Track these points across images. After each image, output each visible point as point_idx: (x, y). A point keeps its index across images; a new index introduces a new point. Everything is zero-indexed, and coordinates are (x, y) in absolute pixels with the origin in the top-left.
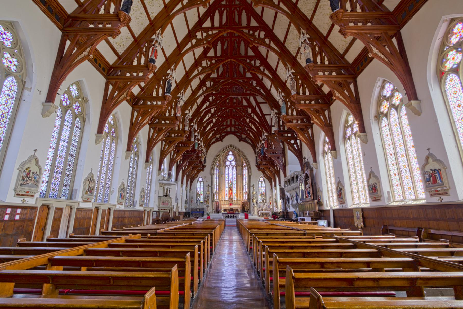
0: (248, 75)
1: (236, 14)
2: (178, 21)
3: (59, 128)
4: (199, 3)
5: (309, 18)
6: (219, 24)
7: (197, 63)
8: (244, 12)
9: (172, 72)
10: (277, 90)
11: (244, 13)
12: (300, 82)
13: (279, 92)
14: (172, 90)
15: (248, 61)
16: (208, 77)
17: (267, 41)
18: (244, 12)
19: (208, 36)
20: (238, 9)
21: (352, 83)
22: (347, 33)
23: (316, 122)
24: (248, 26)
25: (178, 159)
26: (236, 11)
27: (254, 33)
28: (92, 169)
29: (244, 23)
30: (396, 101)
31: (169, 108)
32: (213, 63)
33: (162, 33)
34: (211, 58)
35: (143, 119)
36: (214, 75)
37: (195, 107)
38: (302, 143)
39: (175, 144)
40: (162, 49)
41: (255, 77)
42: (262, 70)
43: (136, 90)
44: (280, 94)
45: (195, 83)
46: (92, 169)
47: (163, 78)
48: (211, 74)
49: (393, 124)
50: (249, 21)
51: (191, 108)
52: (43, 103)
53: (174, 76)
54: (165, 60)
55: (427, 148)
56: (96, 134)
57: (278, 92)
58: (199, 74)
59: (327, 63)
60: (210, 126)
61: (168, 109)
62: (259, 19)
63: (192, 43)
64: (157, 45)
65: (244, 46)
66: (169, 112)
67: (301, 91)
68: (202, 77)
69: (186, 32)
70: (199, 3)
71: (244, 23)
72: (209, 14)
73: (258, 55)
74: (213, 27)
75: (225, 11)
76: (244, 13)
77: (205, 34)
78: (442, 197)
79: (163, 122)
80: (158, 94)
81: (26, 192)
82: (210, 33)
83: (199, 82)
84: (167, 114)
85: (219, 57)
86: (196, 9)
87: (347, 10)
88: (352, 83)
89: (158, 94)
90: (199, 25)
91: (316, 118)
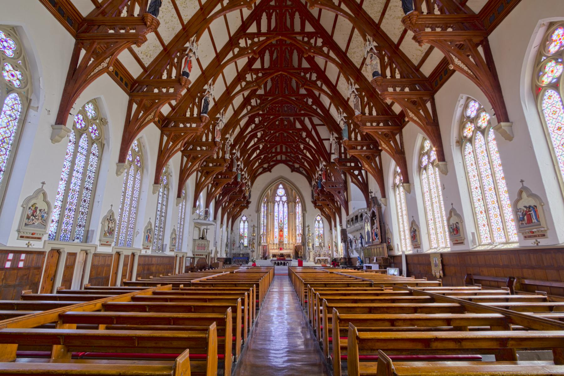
0: (303, 91)
1: (288, 17)
2: (217, 25)
3: (71, 156)
4: (242, 3)
5: (377, 22)
6: (267, 29)
7: (240, 77)
8: (297, 14)
9: (210, 87)
10: (338, 109)
11: (297, 16)
12: (366, 99)
13: (340, 112)
14: (209, 110)
15: (302, 74)
16: (253, 94)
17: (325, 49)
18: (297, 14)
19: (253, 44)
20: (290, 11)
21: (429, 102)
22: (422, 40)
23: (385, 148)
24: (303, 32)
25: (217, 194)
26: (288, 14)
27: (309, 41)
28: (112, 206)
29: (298, 28)
30: (482, 123)
31: (206, 131)
32: (259, 77)
33: (197, 40)
34: (257, 71)
35: (174, 145)
36: (261, 92)
37: (237, 130)
38: (368, 173)
39: (213, 175)
40: (198, 60)
41: (310, 94)
42: (319, 85)
43: (165, 110)
44: (341, 114)
45: (238, 101)
46: (112, 206)
47: (199, 95)
48: (257, 90)
49: (478, 151)
50: (303, 26)
51: (233, 131)
52: (52, 126)
53: (211, 92)
54: (201, 73)
55: (520, 180)
56: (117, 164)
57: (338, 112)
58: (242, 90)
59: (398, 76)
60: (255, 153)
61: (205, 133)
62: (316, 23)
63: (233, 53)
64: (191, 54)
65: (297, 56)
66: (206, 137)
67: (367, 111)
68: (246, 93)
69: (227, 39)
70: (242, 3)
71: (298, 28)
72: (255, 17)
73: (315, 67)
74: (259, 33)
75: (274, 14)
76: (297, 16)
77: (249, 42)
78: (538, 240)
79: (199, 149)
80: (192, 114)
81: (32, 234)
82: (256, 40)
83: (243, 100)
84: (204, 139)
85: (266, 69)
86: (239, 11)
87: (423, 12)
88: (429, 102)
89: (192, 114)
90: (242, 31)
91: (385, 144)
